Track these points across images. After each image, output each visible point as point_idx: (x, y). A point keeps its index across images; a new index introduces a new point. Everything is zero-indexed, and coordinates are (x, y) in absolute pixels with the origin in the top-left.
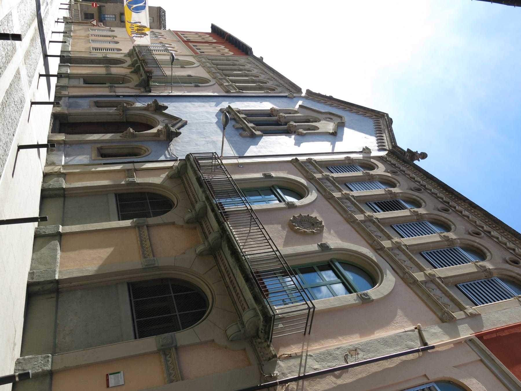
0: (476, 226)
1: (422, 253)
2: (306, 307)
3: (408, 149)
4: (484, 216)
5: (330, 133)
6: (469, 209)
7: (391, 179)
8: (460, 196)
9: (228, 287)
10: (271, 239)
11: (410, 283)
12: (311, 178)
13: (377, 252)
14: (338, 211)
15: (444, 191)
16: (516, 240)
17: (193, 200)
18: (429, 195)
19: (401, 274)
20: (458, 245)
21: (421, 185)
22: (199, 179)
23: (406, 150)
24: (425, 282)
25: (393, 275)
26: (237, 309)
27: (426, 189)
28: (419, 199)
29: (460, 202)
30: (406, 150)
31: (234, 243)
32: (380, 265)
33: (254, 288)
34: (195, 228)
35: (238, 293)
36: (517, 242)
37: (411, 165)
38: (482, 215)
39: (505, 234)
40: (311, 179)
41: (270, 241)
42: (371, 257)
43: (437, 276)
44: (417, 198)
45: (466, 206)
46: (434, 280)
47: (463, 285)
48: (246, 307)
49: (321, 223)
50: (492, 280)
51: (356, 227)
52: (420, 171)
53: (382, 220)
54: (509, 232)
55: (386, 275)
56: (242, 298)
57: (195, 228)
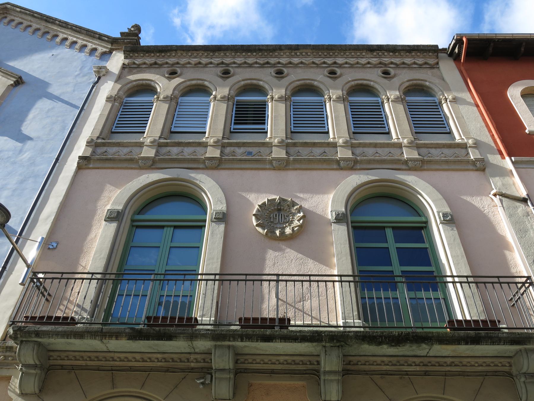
0: (274, 66)
1: (113, 130)
2: (337, 284)
3: (122, 34)
4: (314, 51)
5: (12, 85)
6: (293, 54)
7: (188, 83)
8: (271, 48)
9: (426, 373)
10: (63, 273)
11: (421, 167)
12: (151, 162)
13: (355, 169)
14: (252, 169)
15: (249, 54)
16: (361, 53)
17: (418, 368)
18: (192, 69)
19: (404, 167)
20: (124, 97)
21: (173, 65)
22: (136, 335)
23: (119, 36)
24: (157, 153)
25: (409, 175)
26: (183, 370)
27: (340, 66)
28: (249, 82)
29: (276, 54)
30: (119, 36)
31: (331, 332)
32: (182, 177)
33: (497, 337)
34: (250, 385)
35: (97, 357)
36: (364, 54)
37: (176, 50)
38: (311, 51)
39: (347, 54)
40: (152, 165)
41: (65, 276)
42: (367, 180)
43: (95, 139)
44: (246, 82)
45: (288, 54)
46: (96, 143)
47: (116, 127)
48: (508, 360)
49: (282, 200)
50: (125, 103)
51: (298, 166)
52: (196, 50)
53: (103, 134)
54: (349, 50)
55: (195, 179)
56: (130, 356)
57: (250, 385)
